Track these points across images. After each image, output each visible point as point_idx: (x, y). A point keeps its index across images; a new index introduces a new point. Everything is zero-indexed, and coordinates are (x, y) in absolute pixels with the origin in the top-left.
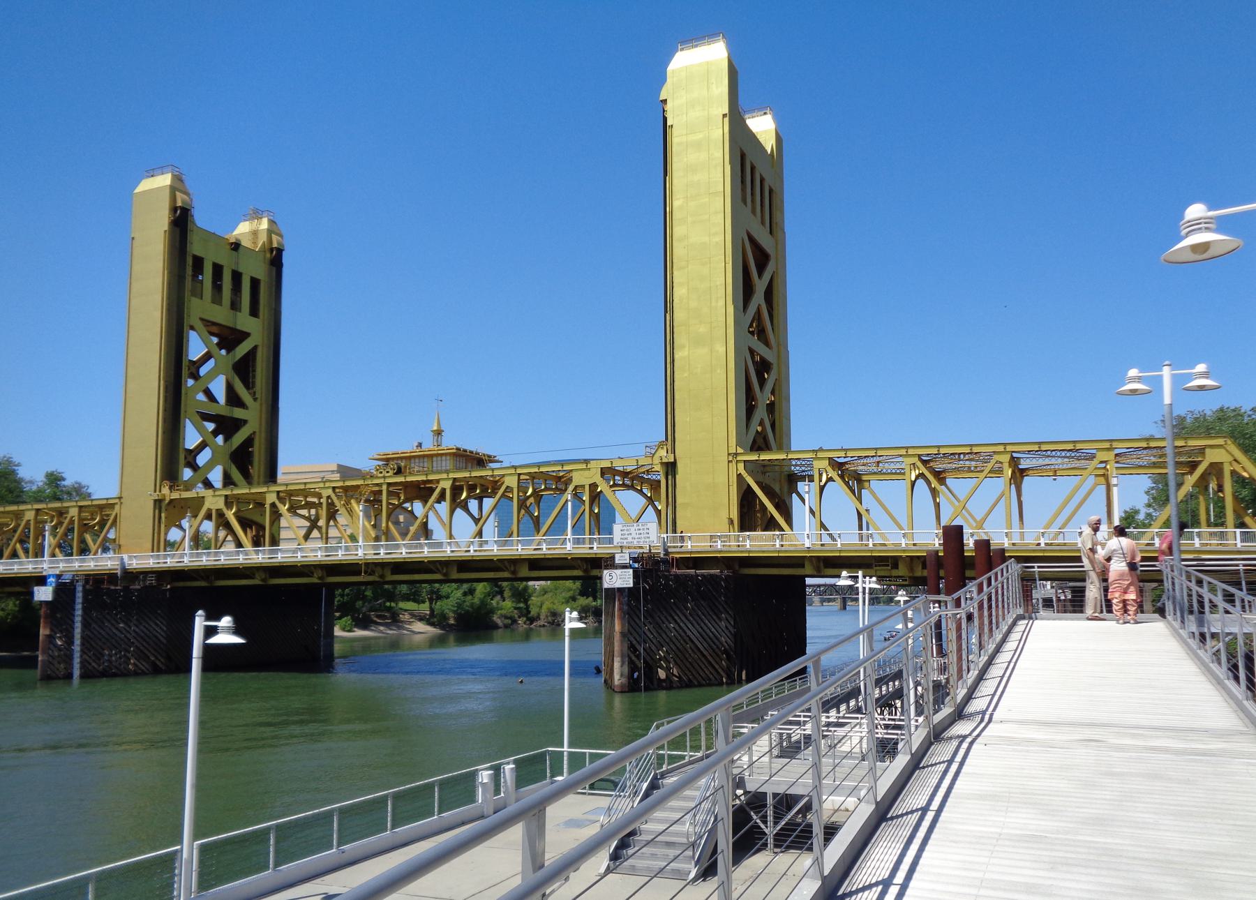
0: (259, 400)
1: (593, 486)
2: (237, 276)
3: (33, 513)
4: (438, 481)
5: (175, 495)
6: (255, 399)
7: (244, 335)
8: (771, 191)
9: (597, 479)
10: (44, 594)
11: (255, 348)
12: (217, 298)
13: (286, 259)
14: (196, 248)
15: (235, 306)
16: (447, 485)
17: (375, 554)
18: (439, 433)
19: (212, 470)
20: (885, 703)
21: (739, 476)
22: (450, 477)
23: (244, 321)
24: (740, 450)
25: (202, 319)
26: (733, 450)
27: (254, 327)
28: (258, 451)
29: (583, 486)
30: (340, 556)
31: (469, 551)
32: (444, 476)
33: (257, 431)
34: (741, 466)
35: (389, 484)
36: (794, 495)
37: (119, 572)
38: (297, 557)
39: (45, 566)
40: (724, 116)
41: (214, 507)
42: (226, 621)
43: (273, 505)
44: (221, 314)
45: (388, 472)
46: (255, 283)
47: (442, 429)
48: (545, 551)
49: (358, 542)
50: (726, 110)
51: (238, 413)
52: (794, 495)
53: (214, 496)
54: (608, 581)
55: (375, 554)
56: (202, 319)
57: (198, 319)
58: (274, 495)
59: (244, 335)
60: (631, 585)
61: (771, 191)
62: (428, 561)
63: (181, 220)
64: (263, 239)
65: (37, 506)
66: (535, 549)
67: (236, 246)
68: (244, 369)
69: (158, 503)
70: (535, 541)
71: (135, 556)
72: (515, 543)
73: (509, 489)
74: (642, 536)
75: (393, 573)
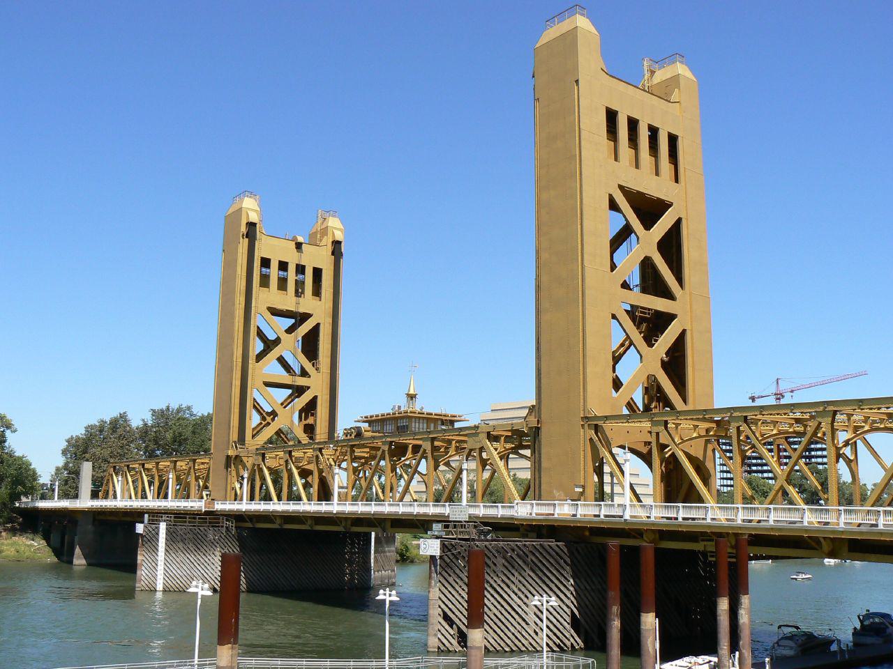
2: (301, 269)
8: (673, 139)
23: (307, 303)
27: (318, 310)
44: (287, 301)
46: (317, 273)
51: (301, 381)
68: (310, 346)
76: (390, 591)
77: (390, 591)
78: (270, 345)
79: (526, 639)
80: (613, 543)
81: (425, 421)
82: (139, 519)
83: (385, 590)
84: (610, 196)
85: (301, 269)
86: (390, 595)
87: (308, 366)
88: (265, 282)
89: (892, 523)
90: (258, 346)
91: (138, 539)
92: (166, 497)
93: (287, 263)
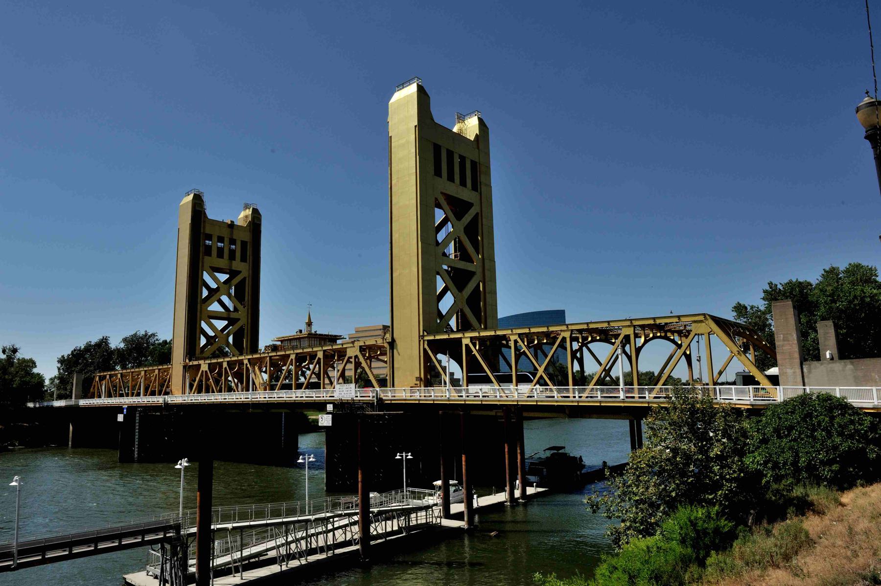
1: (356, 357)
3: (322, 352)
5: (191, 364)
7: (239, 272)
8: (474, 164)
9: (358, 353)
10: (120, 418)
11: (245, 279)
12: (451, 178)
15: (451, 178)
18: (309, 324)
19: (473, 313)
20: (697, 582)
21: (425, 350)
23: (237, 265)
24: (425, 334)
25: (442, 193)
30: (433, 397)
31: (303, 397)
32: (292, 352)
35: (270, 357)
38: (597, 397)
40: (416, 126)
41: (204, 370)
42: (410, 454)
43: (226, 368)
46: (244, 244)
49: (619, 386)
50: (416, 123)
53: (204, 364)
56: (442, 193)
57: (440, 194)
58: (469, 340)
59: (239, 272)
60: (331, 425)
65: (145, 369)
66: (330, 397)
68: (239, 297)
69: (184, 367)
70: (655, 390)
73: (319, 359)
74: (348, 392)
85: (233, 241)
89: (880, 401)
92: (138, 395)
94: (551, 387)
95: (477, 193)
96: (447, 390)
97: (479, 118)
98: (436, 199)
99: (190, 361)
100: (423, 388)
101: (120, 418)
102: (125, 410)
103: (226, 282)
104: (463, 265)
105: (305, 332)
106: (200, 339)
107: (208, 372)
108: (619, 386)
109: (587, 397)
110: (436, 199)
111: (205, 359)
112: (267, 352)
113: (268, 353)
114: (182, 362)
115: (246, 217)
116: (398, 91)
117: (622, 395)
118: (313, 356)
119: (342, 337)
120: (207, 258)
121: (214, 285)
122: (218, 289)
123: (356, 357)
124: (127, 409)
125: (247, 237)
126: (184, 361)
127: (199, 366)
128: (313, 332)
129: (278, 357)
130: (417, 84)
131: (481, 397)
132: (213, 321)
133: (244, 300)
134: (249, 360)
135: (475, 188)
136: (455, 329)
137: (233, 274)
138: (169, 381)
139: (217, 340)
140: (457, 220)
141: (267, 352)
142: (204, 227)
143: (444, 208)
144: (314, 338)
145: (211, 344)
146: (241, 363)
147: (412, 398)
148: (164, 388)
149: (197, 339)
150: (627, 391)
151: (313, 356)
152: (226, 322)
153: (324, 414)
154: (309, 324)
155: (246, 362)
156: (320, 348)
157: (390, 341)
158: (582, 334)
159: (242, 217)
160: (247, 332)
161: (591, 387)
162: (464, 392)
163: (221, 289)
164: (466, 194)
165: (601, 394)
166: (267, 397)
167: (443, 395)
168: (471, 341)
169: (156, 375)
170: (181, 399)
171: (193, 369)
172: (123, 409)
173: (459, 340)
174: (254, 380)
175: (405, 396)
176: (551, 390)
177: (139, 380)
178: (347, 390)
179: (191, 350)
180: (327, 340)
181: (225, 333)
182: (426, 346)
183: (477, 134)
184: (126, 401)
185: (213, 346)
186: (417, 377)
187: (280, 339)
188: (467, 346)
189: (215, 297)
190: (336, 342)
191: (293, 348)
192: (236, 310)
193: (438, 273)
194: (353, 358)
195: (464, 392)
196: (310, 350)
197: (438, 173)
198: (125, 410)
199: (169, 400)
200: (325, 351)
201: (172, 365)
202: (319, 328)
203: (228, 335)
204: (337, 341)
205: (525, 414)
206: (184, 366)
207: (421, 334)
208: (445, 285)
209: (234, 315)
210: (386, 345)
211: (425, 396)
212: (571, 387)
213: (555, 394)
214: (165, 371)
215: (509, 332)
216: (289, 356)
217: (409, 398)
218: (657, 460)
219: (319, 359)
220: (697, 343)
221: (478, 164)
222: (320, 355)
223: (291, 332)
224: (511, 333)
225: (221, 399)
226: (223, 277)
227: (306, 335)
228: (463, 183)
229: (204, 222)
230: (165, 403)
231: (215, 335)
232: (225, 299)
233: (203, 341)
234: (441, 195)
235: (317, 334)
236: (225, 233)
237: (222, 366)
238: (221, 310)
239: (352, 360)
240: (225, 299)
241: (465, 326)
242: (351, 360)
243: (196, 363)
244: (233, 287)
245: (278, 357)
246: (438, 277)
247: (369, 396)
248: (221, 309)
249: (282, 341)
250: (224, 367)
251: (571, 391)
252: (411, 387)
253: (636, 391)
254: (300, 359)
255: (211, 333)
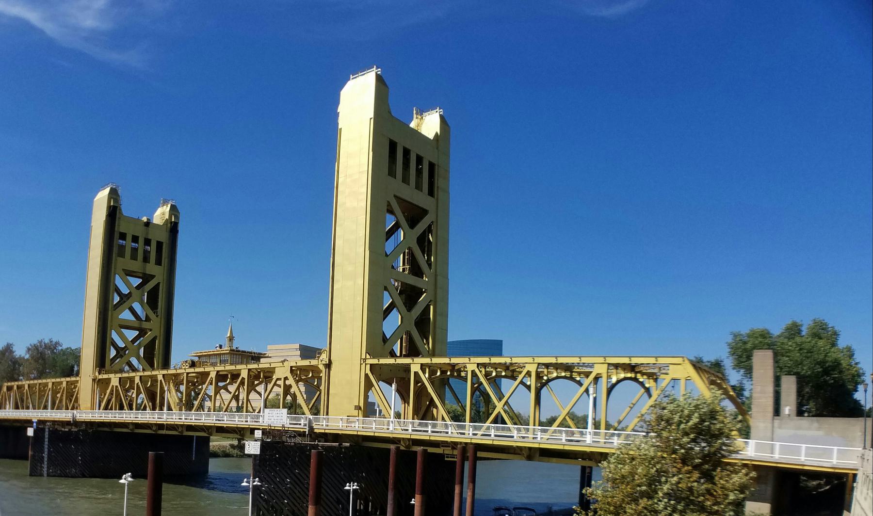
0: (159, 317)
2: (148, 242)
4: (591, 366)
5: (100, 377)
6: (157, 316)
7: (153, 277)
8: (432, 166)
10: (30, 432)
11: (158, 284)
13: (181, 228)
14: (121, 227)
15: (146, 259)
16: (533, 368)
17: (136, 418)
18: (231, 339)
21: (366, 375)
22: (535, 361)
23: (152, 268)
24: (368, 356)
26: (363, 357)
27: (158, 272)
28: (158, 345)
29: (280, 379)
33: (158, 335)
34: (368, 367)
35: (188, 373)
36: (447, 389)
37: (71, 420)
39: (49, 414)
40: (371, 119)
41: (115, 385)
45: (187, 366)
46: (159, 245)
47: (234, 336)
48: (183, 420)
49: (587, 428)
52: (447, 389)
54: (248, 449)
55: (136, 418)
59: (153, 277)
61: (432, 166)
62: (226, 427)
63: (113, 213)
64: (167, 216)
67: (148, 224)
68: (153, 302)
69: (94, 380)
71: (84, 412)
72: (211, 415)
73: (243, 379)
74: (279, 418)
75: (187, 430)
76: (353, 483)
77: (353, 483)
78: (124, 298)
79: (296, 506)
80: (418, 449)
81: (240, 356)
82: (29, 425)
83: (350, 483)
84: (388, 202)
85: (148, 242)
86: (353, 486)
87: (152, 315)
88: (121, 254)
90: (117, 299)
91: (821, 492)
92: (45, 408)
93: (138, 237)
94: (510, 425)
95: (433, 199)
96: (391, 422)
97: (441, 116)
98: (389, 204)
99: (99, 374)
100: (361, 418)
101: (30, 432)
102: (35, 424)
103: (138, 287)
104: (413, 280)
105: (226, 349)
106: (110, 350)
107: (119, 386)
108: (587, 428)
109: (483, 435)
110: (389, 204)
111: (116, 372)
112: (183, 368)
113: (185, 369)
114: (91, 375)
115: (163, 214)
116: (353, 79)
117: (589, 439)
118: (235, 376)
119: (267, 355)
120: (120, 259)
121: (125, 291)
122: (129, 295)
123: (286, 379)
124: (37, 423)
125: (164, 237)
126: (94, 373)
127: (109, 380)
128: (234, 348)
129: (194, 375)
130: (376, 73)
131: (429, 432)
132: (124, 331)
133: (157, 308)
134: (164, 375)
135: (431, 193)
136: (398, 355)
137: (146, 278)
138: (77, 394)
139: (127, 352)
140: (410, 228)
141: (183, 368)
142: (119, 226)
143: (397, 214)
144: (236, 354)
145: (122, 357)
146: (154, 379)
147: (349, 428)
148: (71, 399)
149: (107, 350)
150: (596, 434)
151: (235, 376)
152: (137, 333)
153: (252, 441)
154: (231, 339)
155: (160, 378)
156: (244, 366)
157: (328, 363)
158: (548, 369)
159: (161, 215)
160: (158, 345)
161: (487, 424)
162: (430, 427)
163: (133, 295)
164: (421, 199)
165: (517, 434)
166: (117, 416)
167: (384, 427)
168: (421, 368)
169: (64, 387)
170: (90, 415)
171: (102, 383)
172: (33, 422)
173: (407, 368)
174: (169, 398)
175: (342, 426)
176: (509, 429)
177: (59, 395)
178: (277, 415)
179: (101, 363)
180: (250, 358)
181: (135, 344)
182: (368, 371)
183: (437, 133)
184: (35, 415)
185: (123, 358)
186: (355, 406)
187: (198, 354)
188: (416, 373)
189: (127, 304)
190: (260, 361)
191: (214, 365)
192: (148, 319)
193: (386, 289)
194: (283, 380)
195: (430, 427)
196: (233, 367)
197: (392, 173)
198: (35, 424)
199: (78, 415)
200: (249, 370)
201: (80, 377)
202: (242, 345)
203: (139, 346)
204: (261, 359)
205: (480, 454)
206: (93, 379)
207: (363, 357)
208: (391, 300)
209: (146, 325)
210: (321, 367)
211: (363, 427)
212: (467, 423)
213: (515, 433)
214: (72, 384)
215: (466, 360)
216: (208, 374)
217: (345, 428)
218: (722, 506)
219: (243, 379)
220: (629, 409)
221: (436, 167)
222: (244, 374)
223: (212, 349)
224: (468, 362)
225: (111, 417)
226: (136, 282)
227: (228, 352)
228: (418, 187)
229: (119, 218)
230: (73, 419)
231: (126, 347)
232: (137, 306)
233: (113, 353)
234: (394, 199)
235: (239, 351)
236: (140, 232)
237: (134, 381)
238: (133, 318)
239: (280, 383)
240: (137, 306)
241: (413, 351)
242: (278, 382)
243: (105, 376)
244: (146, 294)
245: (194, 375)
246: (386, 293)
247: (300, 424)
248: (131, 318)
249: (199, 357)
250: (136, 382)
251: (531, 431)
252: (348, 416)
253: (603, 435)
254: (221, 377)
255: (121, 344)
